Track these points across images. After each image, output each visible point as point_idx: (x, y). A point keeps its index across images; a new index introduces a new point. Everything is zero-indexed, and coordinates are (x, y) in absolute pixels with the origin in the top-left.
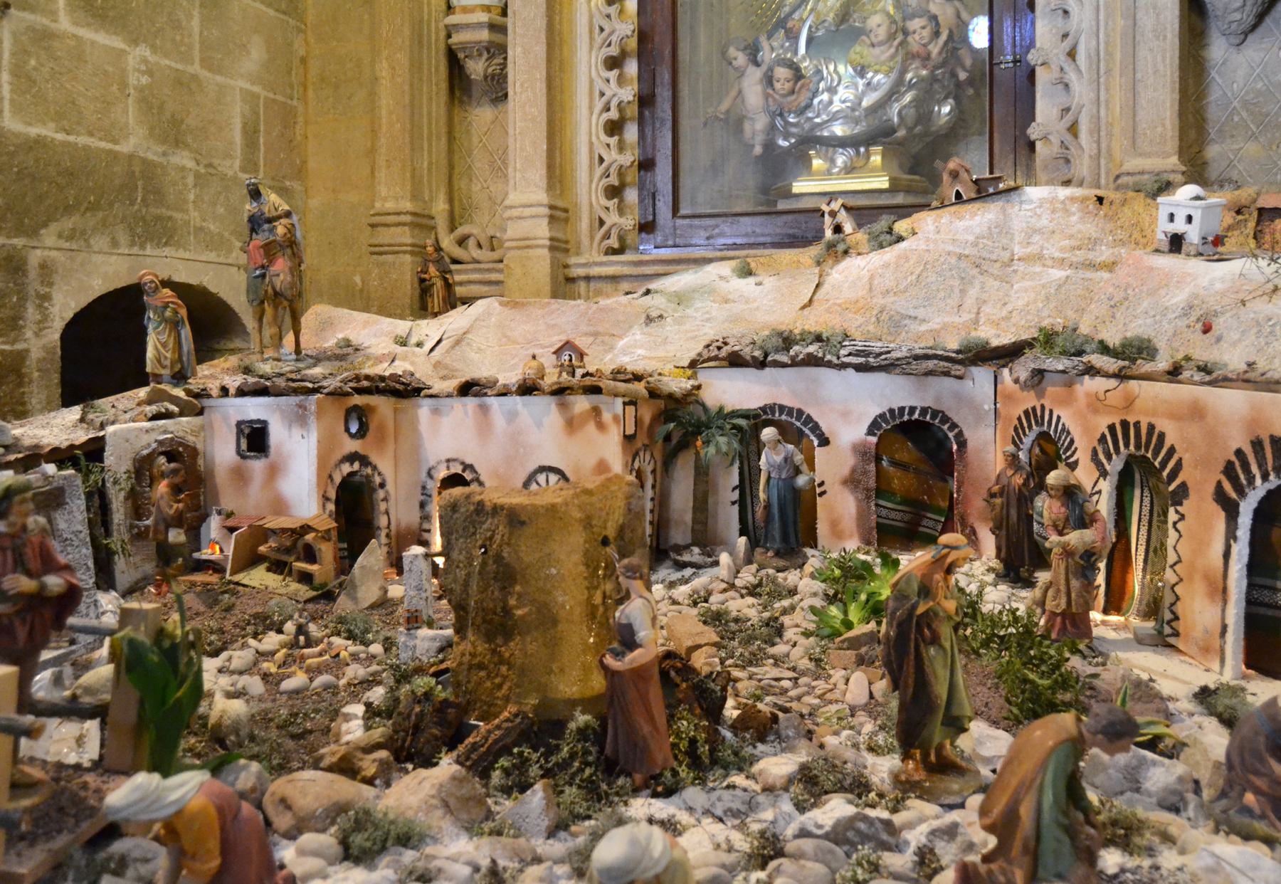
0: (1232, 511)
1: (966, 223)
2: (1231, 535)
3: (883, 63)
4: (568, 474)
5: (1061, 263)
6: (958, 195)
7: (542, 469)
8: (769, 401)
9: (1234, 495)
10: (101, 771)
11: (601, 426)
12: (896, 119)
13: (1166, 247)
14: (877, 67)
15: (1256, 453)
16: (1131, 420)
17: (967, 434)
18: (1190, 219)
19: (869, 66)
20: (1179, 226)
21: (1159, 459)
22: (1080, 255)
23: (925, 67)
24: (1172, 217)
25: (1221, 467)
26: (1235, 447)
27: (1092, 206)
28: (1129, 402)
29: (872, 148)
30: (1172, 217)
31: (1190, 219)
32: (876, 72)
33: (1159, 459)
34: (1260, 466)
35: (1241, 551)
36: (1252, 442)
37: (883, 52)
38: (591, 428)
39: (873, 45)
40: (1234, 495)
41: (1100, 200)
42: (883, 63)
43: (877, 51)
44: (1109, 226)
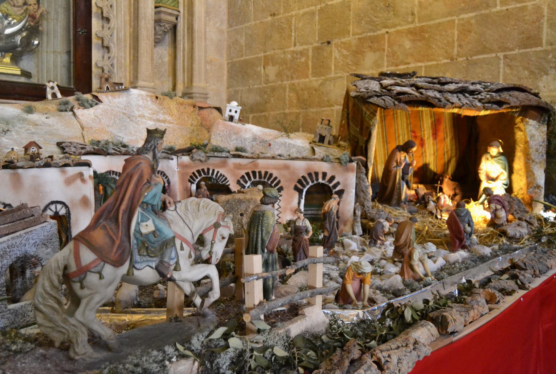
0: (300, 192)
1: (116, 100)
2: (300, 197)
3: (17, 15)
4: (67, 203)
5: (151, 119)
6: (108, 88)
7: (53, 203)
8: (109, 170)
9: (301, 188)
10: (225, 273)
11: (83, 181)
12: (19, 43)
13: (228, 119)
14: (15, 17)
15: (309, 176)
16: (257, 171)
17: (170, 179)
18: (236, 112)
19: (11, 15)
20: (233, 113)
21: (271, 180)
22: (155, 117)
23: (33, 22)
24: (230, 111)
25: (297, 180)
26: (302, 175)
27: (154, 99)
28: (256, 165)
29: (7, 54)
30: (230, 111)
31: (236, 112)
32: (13, 19)
33: (271, 180)
34: (311, 180)
35: (303, 201)
36: (308, 174)
37: (19, 11)
38: (79, 182)
39: (14, 6)
40: (301, 188)
41: (157, 98)
42: (17, 15)
43: (16, 9)
44: (161, 107)
